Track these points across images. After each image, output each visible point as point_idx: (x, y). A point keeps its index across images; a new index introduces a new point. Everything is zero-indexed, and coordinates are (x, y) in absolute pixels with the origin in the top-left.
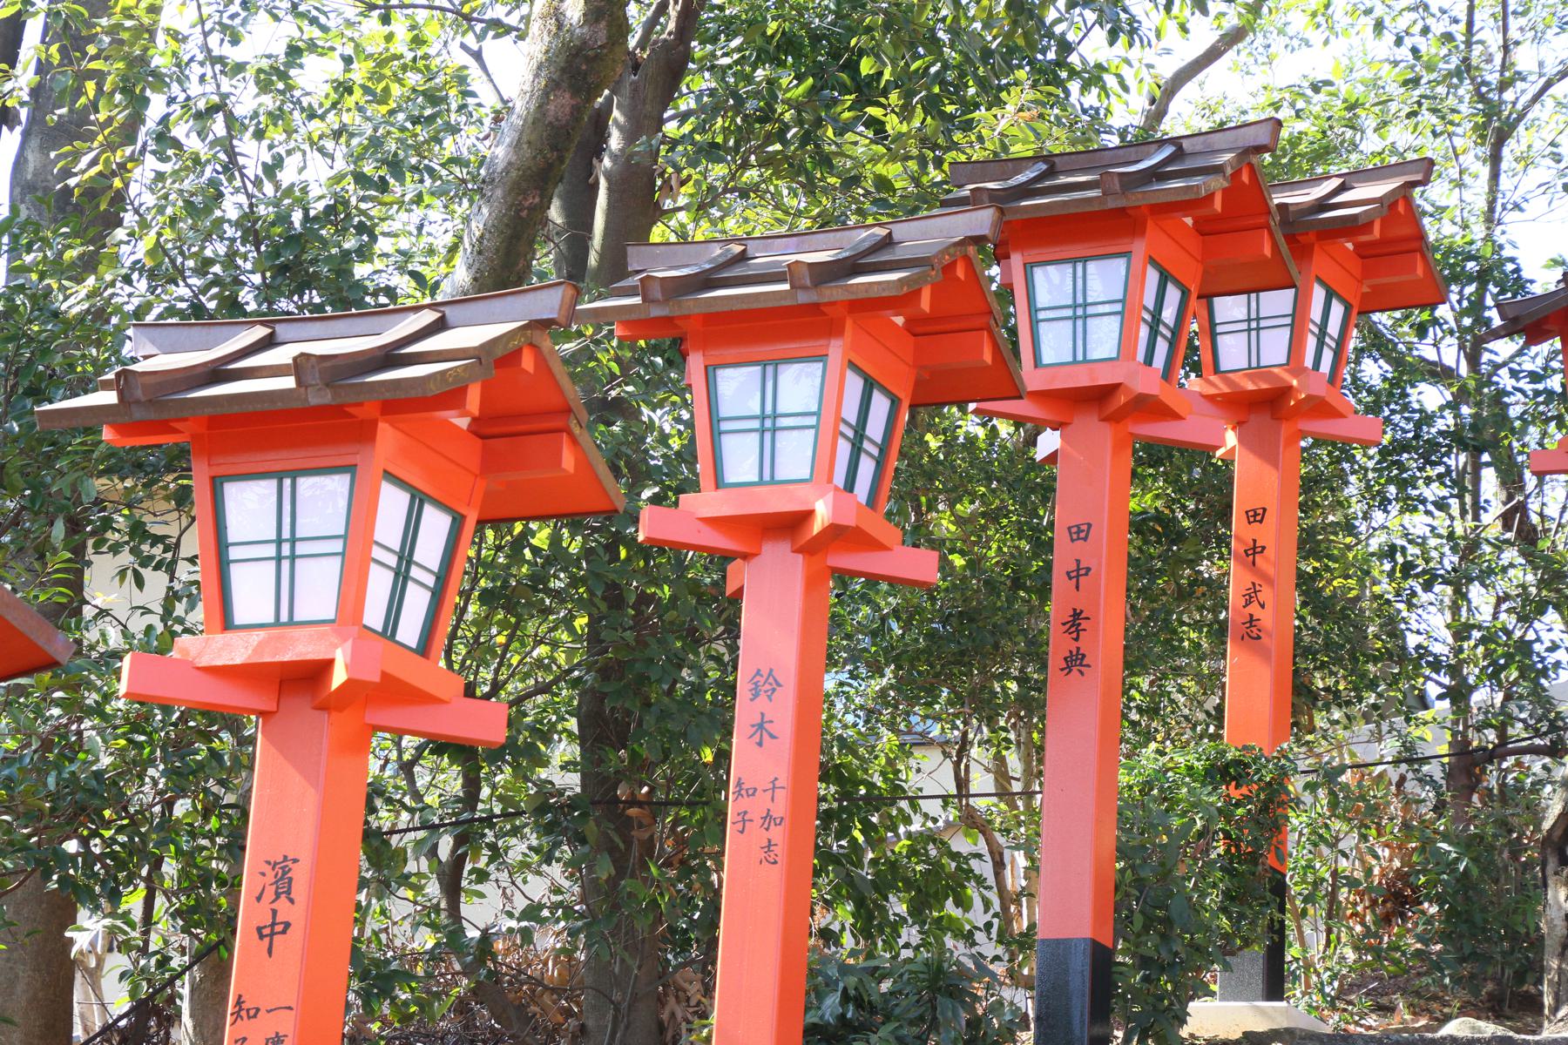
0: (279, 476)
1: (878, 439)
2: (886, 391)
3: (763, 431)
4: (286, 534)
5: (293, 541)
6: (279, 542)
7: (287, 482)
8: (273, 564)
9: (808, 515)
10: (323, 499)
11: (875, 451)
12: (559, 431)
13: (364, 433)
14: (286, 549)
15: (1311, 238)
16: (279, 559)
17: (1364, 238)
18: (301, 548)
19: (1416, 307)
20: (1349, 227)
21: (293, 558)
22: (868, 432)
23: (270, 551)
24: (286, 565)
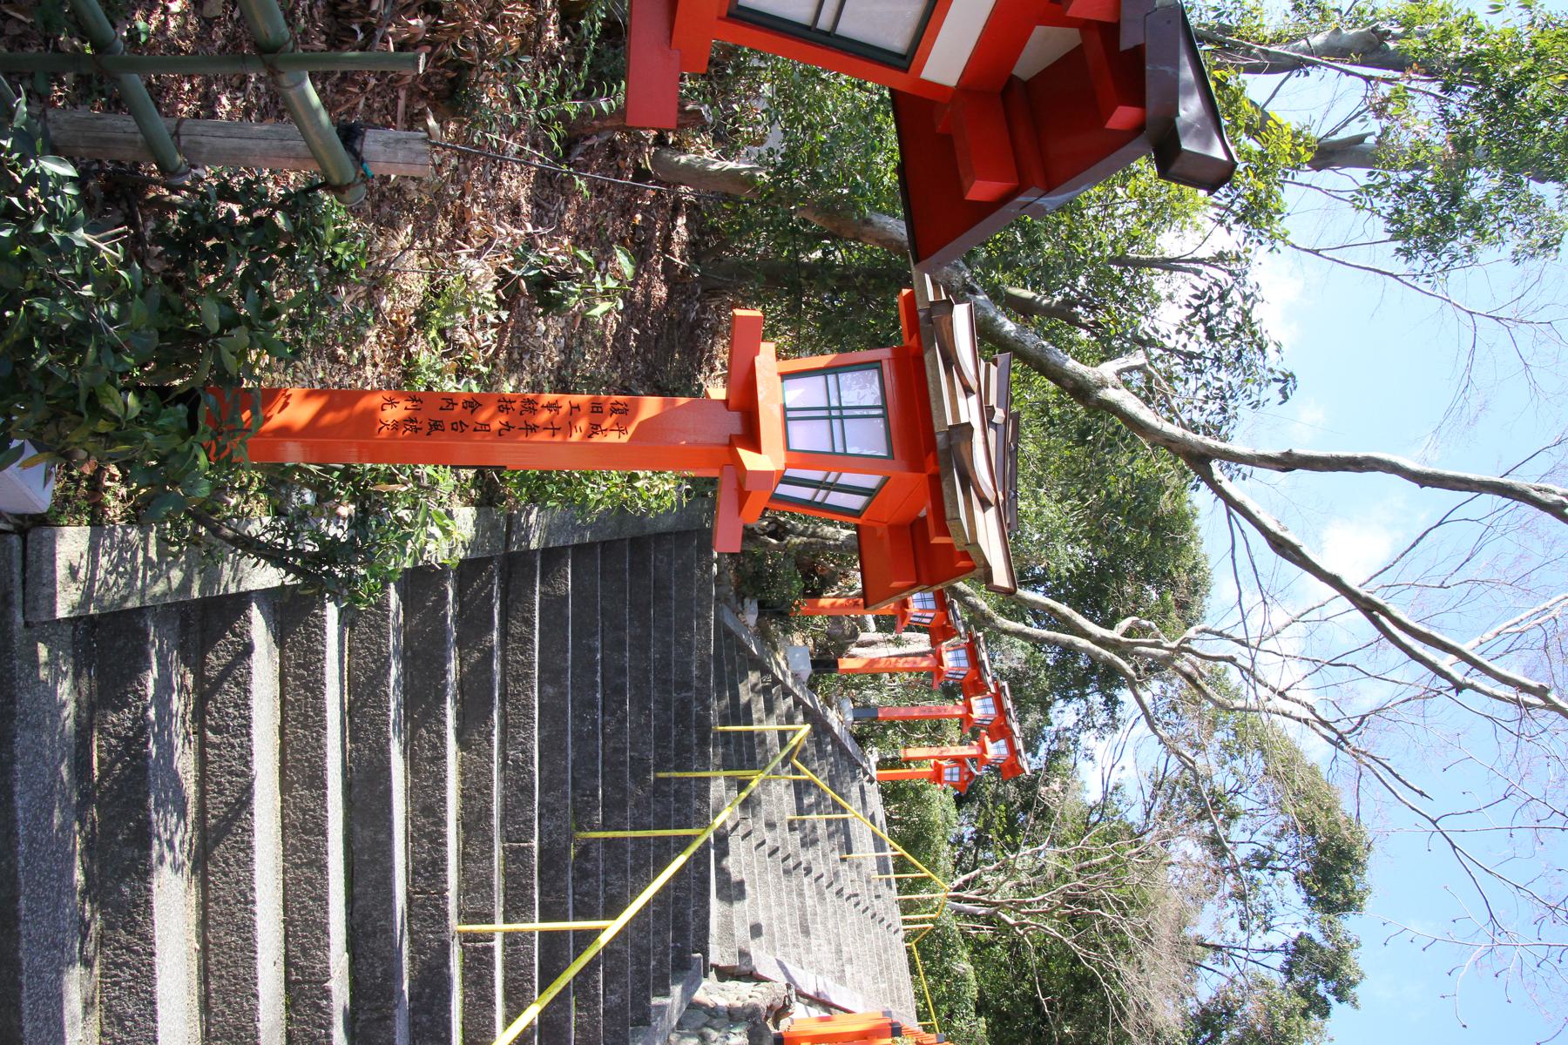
0: (884, 407)
1: (813, 491)
2: (867, 505)
3: (841, 418)
4: (846, 413)
5: (841, 418)
6: (840, 408)
7: (879, 412)
8: (824, 404)
9: (755, 445)
10: (868, 438)
11: (818, 499)
12: (918, 578)
13: (915, 465)
14: (835, 414)
15: (931, 469)
16: (829, 408)
17: (931, 523)
18: (836, 423)
19: (730, 359)
20: (941, 516)
21: (830, 418)
22: (832, 493)
23: (834, 403)
24: (825, 413)
